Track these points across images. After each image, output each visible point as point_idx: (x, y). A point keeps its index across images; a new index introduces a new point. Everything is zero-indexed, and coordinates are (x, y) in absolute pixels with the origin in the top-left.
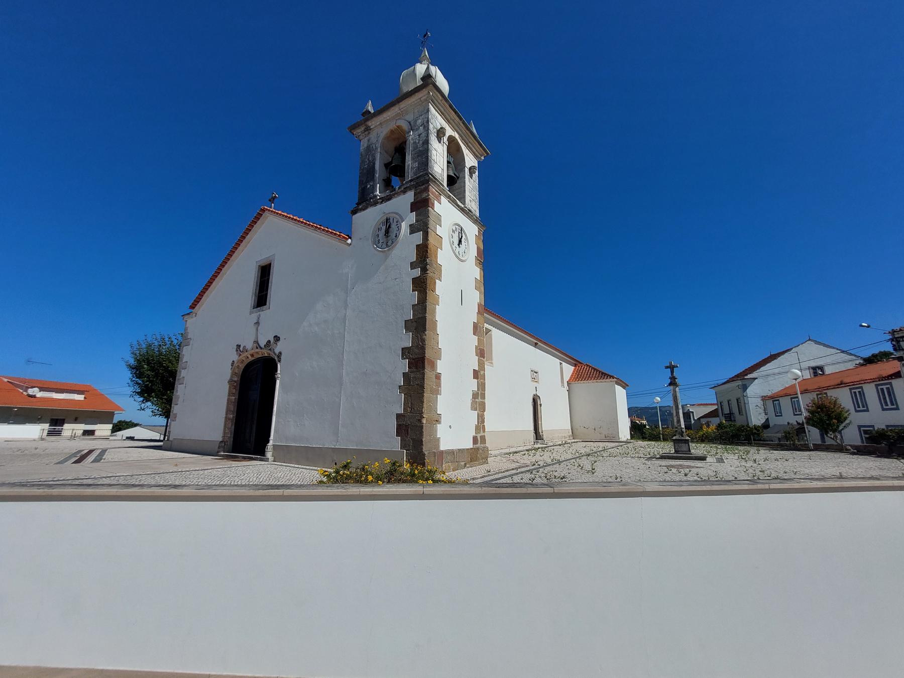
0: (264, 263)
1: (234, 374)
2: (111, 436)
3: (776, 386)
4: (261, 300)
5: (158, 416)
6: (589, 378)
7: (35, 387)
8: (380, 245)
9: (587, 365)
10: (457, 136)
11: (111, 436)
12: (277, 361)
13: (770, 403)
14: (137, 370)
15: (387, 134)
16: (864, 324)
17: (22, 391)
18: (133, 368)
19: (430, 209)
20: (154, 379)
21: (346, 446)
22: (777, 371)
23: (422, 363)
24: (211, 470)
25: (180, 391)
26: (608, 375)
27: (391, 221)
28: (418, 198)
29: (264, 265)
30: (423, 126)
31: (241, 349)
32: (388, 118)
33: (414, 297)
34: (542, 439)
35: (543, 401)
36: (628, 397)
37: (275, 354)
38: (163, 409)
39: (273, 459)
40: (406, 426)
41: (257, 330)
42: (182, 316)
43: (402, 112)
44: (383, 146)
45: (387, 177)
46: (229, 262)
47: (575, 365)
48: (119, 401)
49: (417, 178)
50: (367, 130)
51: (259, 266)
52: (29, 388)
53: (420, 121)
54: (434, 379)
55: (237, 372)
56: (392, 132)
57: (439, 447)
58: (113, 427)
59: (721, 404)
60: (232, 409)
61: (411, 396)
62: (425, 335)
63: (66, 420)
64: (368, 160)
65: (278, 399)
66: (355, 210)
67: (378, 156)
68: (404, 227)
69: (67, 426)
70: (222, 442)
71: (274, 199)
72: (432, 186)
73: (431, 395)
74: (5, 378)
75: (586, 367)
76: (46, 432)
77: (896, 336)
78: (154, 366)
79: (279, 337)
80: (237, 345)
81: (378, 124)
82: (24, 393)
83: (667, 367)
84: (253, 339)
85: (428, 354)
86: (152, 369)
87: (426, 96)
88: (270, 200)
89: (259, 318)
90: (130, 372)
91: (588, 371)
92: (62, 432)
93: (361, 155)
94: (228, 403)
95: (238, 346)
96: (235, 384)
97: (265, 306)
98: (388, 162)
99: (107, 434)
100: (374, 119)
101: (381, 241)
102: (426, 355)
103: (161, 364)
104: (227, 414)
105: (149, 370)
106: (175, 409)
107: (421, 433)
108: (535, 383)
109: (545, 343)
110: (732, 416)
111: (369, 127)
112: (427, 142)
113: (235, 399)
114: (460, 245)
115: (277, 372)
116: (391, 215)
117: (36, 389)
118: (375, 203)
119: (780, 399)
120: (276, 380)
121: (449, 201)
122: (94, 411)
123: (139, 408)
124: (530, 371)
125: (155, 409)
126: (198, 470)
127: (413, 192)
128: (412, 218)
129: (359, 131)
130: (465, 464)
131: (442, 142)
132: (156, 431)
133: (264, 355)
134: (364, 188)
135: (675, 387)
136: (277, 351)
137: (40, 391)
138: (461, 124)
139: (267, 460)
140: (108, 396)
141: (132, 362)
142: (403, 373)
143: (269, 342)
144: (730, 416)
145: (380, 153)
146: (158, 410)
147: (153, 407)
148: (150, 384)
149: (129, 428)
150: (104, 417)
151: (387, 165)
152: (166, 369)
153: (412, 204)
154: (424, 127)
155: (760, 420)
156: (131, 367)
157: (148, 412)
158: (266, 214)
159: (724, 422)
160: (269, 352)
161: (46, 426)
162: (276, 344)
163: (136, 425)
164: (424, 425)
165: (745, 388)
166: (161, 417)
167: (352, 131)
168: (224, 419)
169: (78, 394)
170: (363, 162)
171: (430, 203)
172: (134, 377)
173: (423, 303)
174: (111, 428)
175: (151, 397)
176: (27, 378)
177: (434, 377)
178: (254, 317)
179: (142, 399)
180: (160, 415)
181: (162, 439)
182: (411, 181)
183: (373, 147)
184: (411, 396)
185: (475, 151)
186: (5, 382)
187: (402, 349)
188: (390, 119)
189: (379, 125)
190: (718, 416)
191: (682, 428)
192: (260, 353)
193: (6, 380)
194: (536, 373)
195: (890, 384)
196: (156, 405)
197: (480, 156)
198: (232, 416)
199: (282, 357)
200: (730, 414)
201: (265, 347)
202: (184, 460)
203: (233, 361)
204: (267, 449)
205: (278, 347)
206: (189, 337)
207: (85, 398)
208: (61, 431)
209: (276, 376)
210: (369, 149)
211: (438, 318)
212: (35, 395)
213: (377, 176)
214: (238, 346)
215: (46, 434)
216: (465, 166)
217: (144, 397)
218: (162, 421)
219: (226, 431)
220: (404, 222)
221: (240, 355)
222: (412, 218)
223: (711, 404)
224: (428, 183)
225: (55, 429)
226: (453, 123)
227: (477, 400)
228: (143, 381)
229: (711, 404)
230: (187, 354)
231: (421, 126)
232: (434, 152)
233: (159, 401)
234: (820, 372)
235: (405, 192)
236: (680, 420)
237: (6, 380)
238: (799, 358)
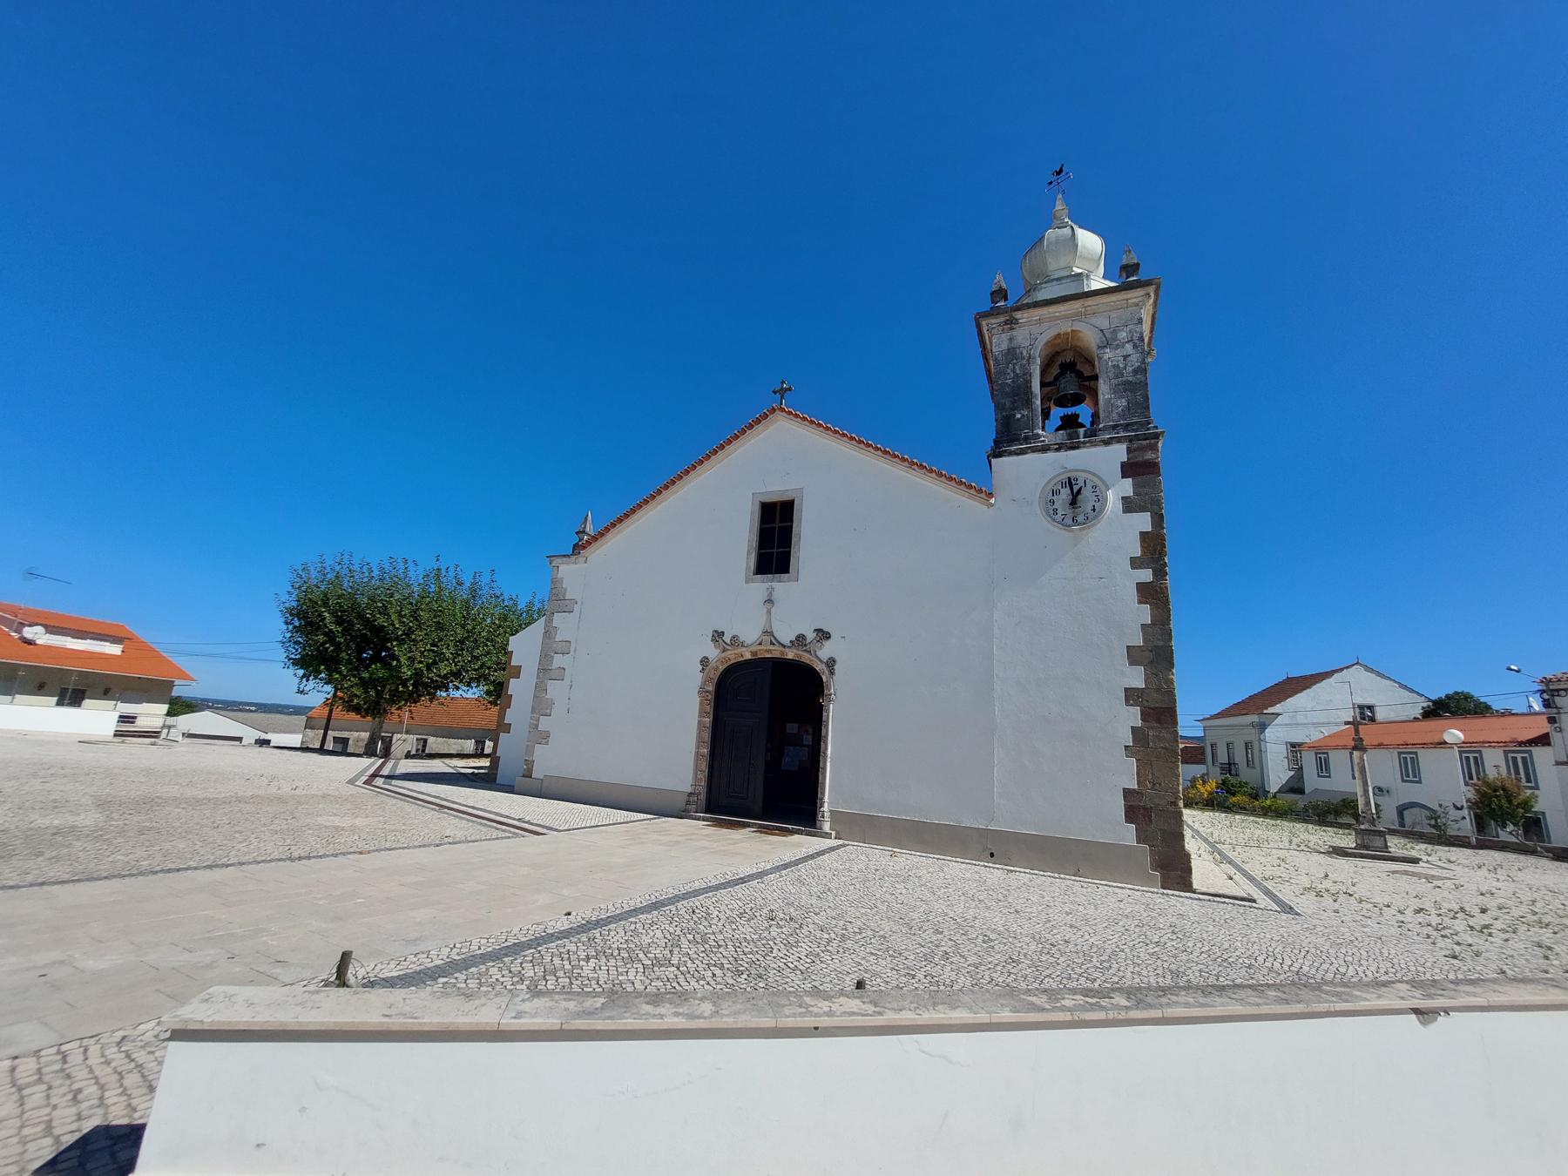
1: (707, 680)
7: (37, 624)
16: (1513, 667)
21: (861, 810)
40: (1146, 809)
41: (769, 612)
62: (1173, 674)
63: (88, 693)
68: (1113, 499)
77: (1551, 687)
87: (1140, 299)
94: (699, 729)
101: (1060, 512)
110: (1233, 767)
111: (1016, 319)
116: (1079, 474)
122: (140, 678)
127: (1125, 446)
132: (240, 720)
148: (332, 648)
153: (1123, 465)
155: (1279, 778)
165: (1262, 727)
169: (73, 638)
173: (1163, 624)
176: (23, 606)
179: (301, 672)
183: (1022, 353)
191: (1373, 814)
195: (1530, 752)
198: (706, 750)
200: (1230, 764)
207: (123, 651)
219: (699, 777)
222: (1127, 487)
231: (1128, 342)
234: (1369, 714)
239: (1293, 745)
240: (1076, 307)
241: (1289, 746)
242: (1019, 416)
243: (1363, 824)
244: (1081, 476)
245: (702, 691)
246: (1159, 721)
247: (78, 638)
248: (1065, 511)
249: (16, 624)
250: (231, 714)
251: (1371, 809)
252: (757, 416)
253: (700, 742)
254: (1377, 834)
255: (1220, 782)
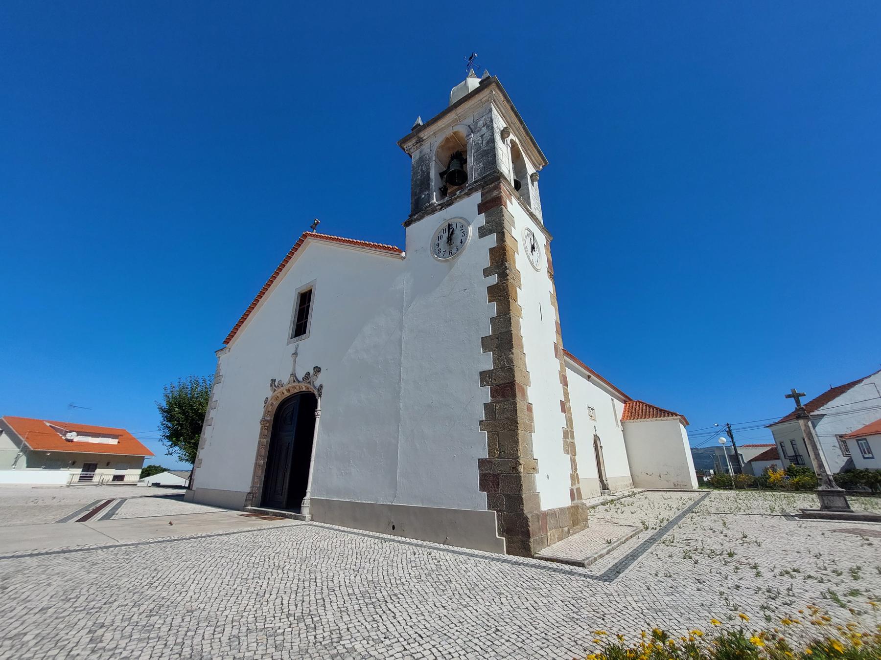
0: (305, 290)
1: (267, 412)
2: (139, 481)
3: (854, 424)
4: (300, 328)
5: (184, 461)
6: (645, 415)
7: (73, 431)
8: (441, 254)
9: (638, 401)
10: (518, 142)
11: (139, 481)
12: (317, 395)
13: (852, 444)
14: (169, 414)
15: (442, 142)
17: (61, 435)
18: (165, 412)
19: (503, 207)
20: (184, 423)
22: (848, 408)
23: (511, 389)
24: (237, 535)
25: (208, 433)
26: (665, 411)
27: (454, 226)
28: (486, 198)
29: (303, 292)
30: (486, 127)
31: (276, 384)
32: (443, 126)
33: (493, 309)
34: (608, 489)
35: (603, 442)
36: (690, 437)
37: (315, 388)
38: (190, 454)
39: (310, 518)
40: (494, 476)
42: (215, 352)
43: (459, 117)
44: (437, 155)
45: (444, 186)
46: (267, 293)
47: (625, 402)
48: (148, 445)
49: (484, 178)
50: (419, 142)
51: (299, 293)
52: (68, 432)
53: (482, 122)
54: (526, 412)
55: (270, 410)
56: (447, 140)
57: (539, 506)
58: (142, 472)
59: (781, 445)
60: (263, 454)
61: (498, 435)
62: (512, 354)
63: (98, 466)
64: (422, 170)
65: (318, 442)
66: (408, 222)
67: (433, 165)
68: (472, 231)
69: (98, 471)
70: (250, 493)
71: (316, 225)
72: (503, 184)
73: (525, 432)
74: (49, 422)
75: (638, 404)
76: (77, 478)
78: (185, 409)
79: (320, 368)
80: (272, 380)
81: (431, 134)
82: (63, 437)
83: (788, 396)
84: (290, 371)
85: (518, 379)
86: (183, 412)
88: (312, 227)
89: (297, 349)
90: (161, 415)
91: (643, 408)
92: (93, 478)
93: (413, 167)
95: (273, 381)
96: (268, 424)
97: (304, 335)
98: (442, 171)
99: (135, 480)
100: (427, 129)
102: (516, 379)
103: (192, 406)
104: (256, 460)
105: (180, 413)
106: (201, 454)
107: (519, 487)
108: (593, 421)
109: (598, 376)
111: (422, 138)
112: (492, 140)
113: (267, 441)
114: (533, 252)
115: (317, 408)
117: (75, 433)
118: (433, 211)
119: (869, 438)
120: (315, 418)
121: (519, 203)
122: (126, 456)
123: (167, 453)
124: (587, 408)
125: (182, 454)
126: (221, 535)
128: (481, 220)
129: (409, 145)
130: (569, 530)
131: (506, 144)
132: (182, 476)
133: (302, 390)
134: (418, 199)
135: (806, 420)
136: (317, 384)
137: (78, 435)
138: (522, 129)
139: (303, 519)
140: (140, 441)
141: (164, 404)
142: (484, 404)
143: (308, 374)
144: (797, 459)
145: (435, 161)
146: (185, 455)
147: (180, 452)
149: (157, 473)
150: (133, 462)
151: (441, 175)
152: (196, 411)
154: (488, 127)
156: (163, 411)
157: (175, 457)
158: (309, 239)
159: (794, 465)
160: (308, 385)
161: (78, 472)
162: (316, 376)
163: (164, 470)
164: (522, 475)
166: (187, 462)
167: (403, 145)
168: (254, 465)
169: (112, 439)
170: (415, 173)
171: (502, 200)
172: (165, 421)
173: (505, 315)
174: (140, 474)
175: (180, 440)
177: (525, 408)
178: (291, 348)
179: (170, 443)
180: (187, 460)
181: (187, 485)
182: (476, 182)
184: (498, 435)
185: (534, 159)
186: (48, 427)
187: (481, 373)
188: (445, 127)
189: (432, 135)
190: (779, 459)
192: (298, 387)
193: (48, 424)
194: (593, 410)
196: (184, 449)
197: (538, 165)
198: (262, 462)
199: (323, 391)
200: (796, 456)
201: (303, 380)
202: (205, 516)
203: (267, 398)
204: (304, 504)
205: (318, 379)
206: (220, 374)
207: (118, 442)
208: (92, 477)
209: (316, 413)
210: (422, 160)
211: (523, 332)
212: (73, 439)
213: (433, 184)
214: (273, 381)
215: (78, 480)
216: (527, 173)
217: (173, 441)
218: (188, 466)
220: (471, 226)
221: (275, 390)
222: (481, 220)
223: (761, 446)
224: (499, 179)
225: (87, 474)
226: (514, 128)
227: (567, 440)
228: (173, 425)
229: (761, 446)
230: (218, 394)
231: (484, 126)
232: (500, 151)
233: (187, 445)
235: (470, 194)
236: (823, 464)
237: (48, 424)
238: (878, 391)
239: (841, 436)
240: (452, 117)
241: (839, 438)
242: (423, 196)
243: (820, 485)
244: (452, 221)
245: (263, 421)
246: (503, 396)
247: (114, 439)
248: (444, 249)
249: (64, 432)
250: (174, 473)
251: (825, 472)
252: (296, 242)
253: (259, 455)
254: (836, 494)
255: (787, 470)
